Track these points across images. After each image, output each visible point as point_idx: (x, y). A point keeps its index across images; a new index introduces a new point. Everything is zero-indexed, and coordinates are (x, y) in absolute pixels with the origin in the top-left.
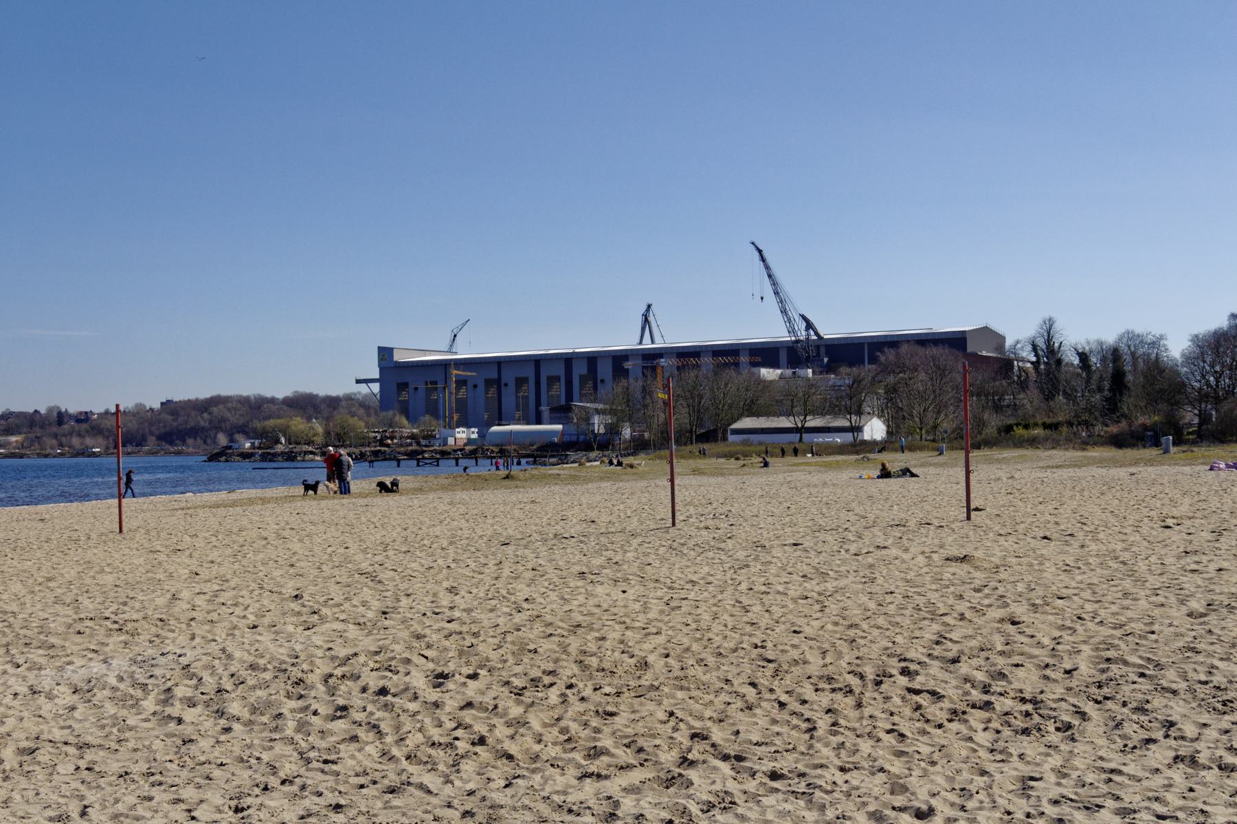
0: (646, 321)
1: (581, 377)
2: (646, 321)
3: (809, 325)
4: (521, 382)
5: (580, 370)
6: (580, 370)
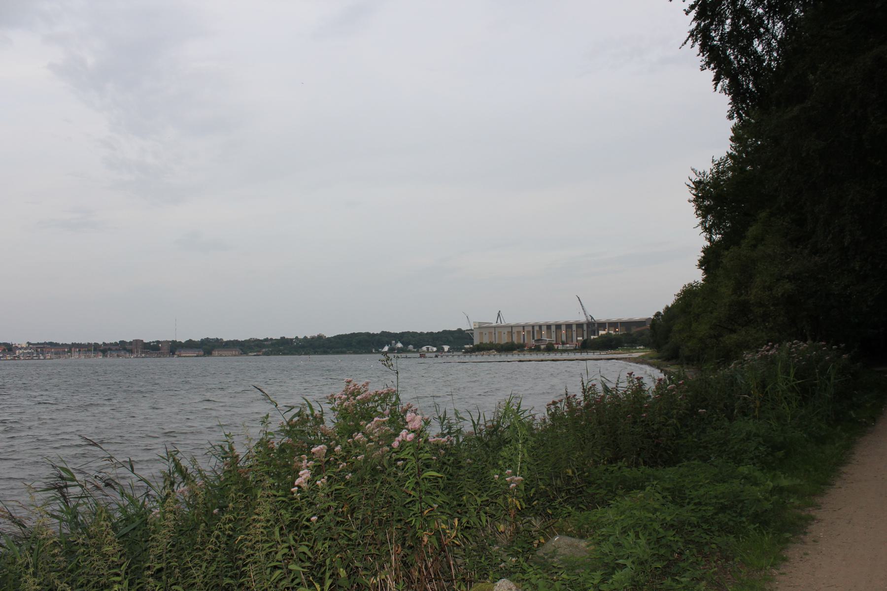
0: (499, 315)
1: (537, 331)
2: (499, 315)
3: (592, 318)
4: (519, 332)
5: (537, 328)
6: (537, 328)
